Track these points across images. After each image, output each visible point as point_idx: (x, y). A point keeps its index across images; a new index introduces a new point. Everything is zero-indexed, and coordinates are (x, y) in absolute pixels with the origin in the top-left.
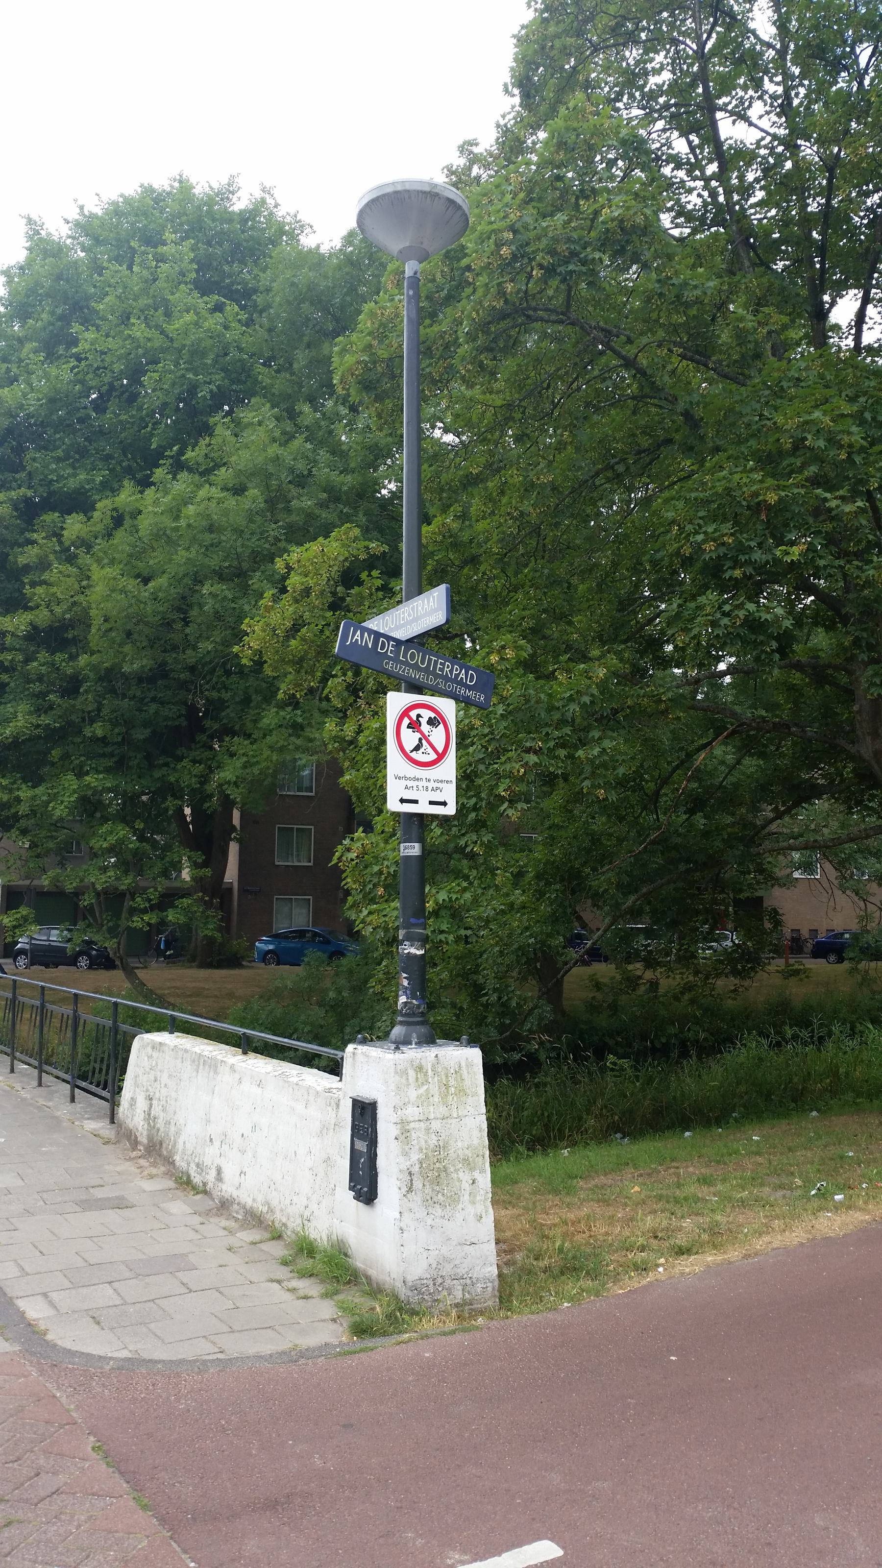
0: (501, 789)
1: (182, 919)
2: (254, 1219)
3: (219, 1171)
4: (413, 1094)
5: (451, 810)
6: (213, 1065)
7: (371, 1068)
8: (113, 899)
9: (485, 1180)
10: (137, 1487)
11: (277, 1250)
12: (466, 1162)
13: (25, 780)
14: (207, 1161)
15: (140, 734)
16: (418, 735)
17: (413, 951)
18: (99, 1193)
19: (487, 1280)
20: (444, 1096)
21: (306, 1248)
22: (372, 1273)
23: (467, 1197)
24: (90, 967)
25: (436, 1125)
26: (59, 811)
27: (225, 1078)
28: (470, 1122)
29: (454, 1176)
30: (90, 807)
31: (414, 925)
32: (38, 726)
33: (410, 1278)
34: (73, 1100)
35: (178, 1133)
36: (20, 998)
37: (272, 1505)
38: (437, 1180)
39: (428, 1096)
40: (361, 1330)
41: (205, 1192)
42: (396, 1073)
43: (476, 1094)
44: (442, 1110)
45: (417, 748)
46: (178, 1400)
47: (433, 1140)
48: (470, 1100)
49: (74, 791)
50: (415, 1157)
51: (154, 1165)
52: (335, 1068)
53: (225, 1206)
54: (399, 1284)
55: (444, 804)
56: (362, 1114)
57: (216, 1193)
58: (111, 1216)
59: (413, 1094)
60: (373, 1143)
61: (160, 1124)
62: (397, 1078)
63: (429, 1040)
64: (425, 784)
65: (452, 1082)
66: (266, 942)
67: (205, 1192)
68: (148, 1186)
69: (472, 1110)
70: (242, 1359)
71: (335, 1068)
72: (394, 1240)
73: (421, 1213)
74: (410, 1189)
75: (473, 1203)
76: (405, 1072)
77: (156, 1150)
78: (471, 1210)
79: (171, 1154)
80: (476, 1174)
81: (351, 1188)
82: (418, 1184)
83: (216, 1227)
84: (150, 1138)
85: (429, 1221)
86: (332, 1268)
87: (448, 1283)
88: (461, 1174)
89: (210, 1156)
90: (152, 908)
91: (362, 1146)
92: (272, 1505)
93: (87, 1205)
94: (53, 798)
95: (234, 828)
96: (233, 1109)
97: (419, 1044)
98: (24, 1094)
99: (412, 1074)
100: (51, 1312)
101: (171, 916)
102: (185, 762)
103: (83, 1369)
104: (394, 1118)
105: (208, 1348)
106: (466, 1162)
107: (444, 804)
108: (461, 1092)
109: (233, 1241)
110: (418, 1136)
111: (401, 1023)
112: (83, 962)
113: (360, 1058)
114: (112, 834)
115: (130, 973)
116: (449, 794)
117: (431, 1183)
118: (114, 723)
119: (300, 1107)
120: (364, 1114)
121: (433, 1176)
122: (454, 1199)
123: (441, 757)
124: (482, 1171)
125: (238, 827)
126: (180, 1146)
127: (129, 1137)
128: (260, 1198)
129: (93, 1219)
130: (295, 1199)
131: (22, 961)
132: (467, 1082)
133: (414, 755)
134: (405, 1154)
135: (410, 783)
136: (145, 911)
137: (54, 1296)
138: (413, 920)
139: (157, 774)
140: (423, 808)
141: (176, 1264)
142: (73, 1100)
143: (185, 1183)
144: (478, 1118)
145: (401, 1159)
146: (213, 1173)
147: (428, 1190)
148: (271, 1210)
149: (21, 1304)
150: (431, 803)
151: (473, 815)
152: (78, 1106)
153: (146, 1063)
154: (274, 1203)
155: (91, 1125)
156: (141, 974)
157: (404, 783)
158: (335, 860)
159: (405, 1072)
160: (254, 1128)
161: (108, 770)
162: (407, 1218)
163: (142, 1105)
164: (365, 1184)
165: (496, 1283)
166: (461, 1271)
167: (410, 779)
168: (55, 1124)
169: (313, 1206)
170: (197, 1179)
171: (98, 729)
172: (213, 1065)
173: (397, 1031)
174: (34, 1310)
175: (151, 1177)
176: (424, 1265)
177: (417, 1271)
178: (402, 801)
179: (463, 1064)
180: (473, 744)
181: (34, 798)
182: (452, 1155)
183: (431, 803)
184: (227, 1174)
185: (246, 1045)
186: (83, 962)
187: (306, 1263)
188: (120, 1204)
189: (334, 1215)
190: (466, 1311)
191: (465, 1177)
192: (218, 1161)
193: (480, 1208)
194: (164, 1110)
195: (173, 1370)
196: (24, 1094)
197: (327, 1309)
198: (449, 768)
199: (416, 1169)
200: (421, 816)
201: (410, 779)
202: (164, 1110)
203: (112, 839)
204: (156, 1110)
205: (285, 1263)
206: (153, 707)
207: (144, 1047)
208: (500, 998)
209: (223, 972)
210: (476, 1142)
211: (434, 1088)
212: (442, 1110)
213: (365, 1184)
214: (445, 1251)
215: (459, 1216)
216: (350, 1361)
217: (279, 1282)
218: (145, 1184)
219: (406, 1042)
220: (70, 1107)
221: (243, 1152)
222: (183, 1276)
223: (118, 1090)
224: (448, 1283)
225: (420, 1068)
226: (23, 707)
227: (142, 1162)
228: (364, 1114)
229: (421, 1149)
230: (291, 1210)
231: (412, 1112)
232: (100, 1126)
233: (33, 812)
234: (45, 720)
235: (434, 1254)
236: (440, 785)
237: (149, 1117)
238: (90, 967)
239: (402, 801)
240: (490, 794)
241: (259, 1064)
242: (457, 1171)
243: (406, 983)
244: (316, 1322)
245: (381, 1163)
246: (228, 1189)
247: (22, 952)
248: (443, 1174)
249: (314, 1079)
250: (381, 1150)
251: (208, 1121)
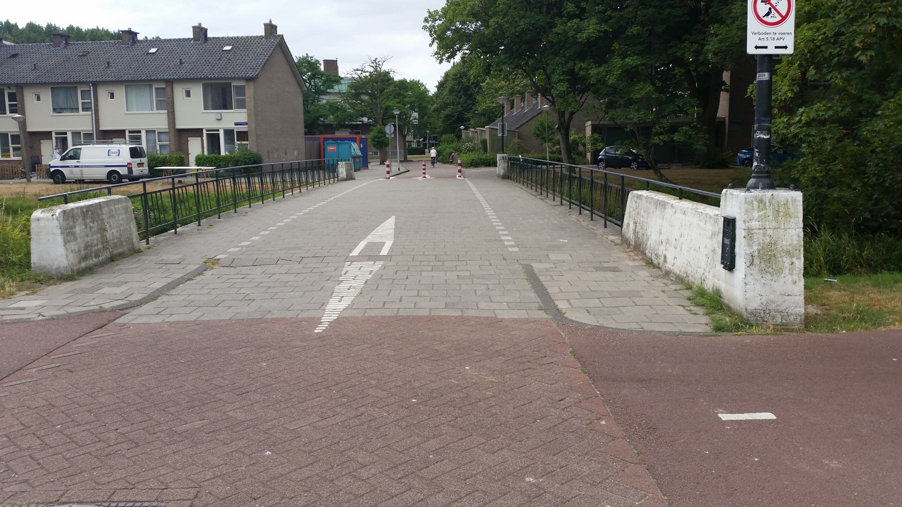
0: (857, 42)
1: (682, 139)
2: (680, 280)
3: (665, 257)
4: (756, 215)
5: (790, 51)
6: (663, 205)
7: (734, 201)
8: (646, 129)
9: (800, 263)
10: (584, 364)
11: (688, 293)
12: (789, 253)
13: (595, 63)
14: (660, 253)
15: (659, 29)
16: (769, 6)
17: (762, 136)
18: (606, 265)
19: (796, 314)
20: (776, 217)
21: (702, 293)
22: (732, 305)
23: (787, 271)
24: (638, 168)
25: (769, 232)
26: (611, 80)
27: (669, 211)
28: (793, 233)
29: (780, 259)
30: (631, 76)
31: (764, 121)
32: (600, 31)
33: (749, 308)
34: (606, 226)
35: (647, 239)
36: (595, 180)
37: (641, 381)
38: (769, 261)
39: (766, 216)
40: (719, 329)
41: (659, 268)
42: (746, 203)
43: (797, 217)
44: (774, 224)
45: (768, 14)
46: (613, 341)
47: (768, 240)
48: (793, 220)
49: (620, 68)
50: (755, 248)
51: (636, 255)
52: (716, 203)
53: (667, 274)
54: (744, 311)
55: (786, 47)
56: (728, 225)
57: (663, 268)
58: (609, 274)
59: (756, 215)
60: (733, 239)
61: (640, 235)
62: (747, 206)
63: (772, 187)
64: (772, 36)
65: (782, 209)
66: (745, 153)
67: (659, 268)
68: (631, 263)
69: (794, 226)
70: (651, 331)
71: (716, 203)
72: (741, 288)
73: (758, 276)
74: (752, 264)
75: (791, 274)
76: (751, 203)
77: (637, 248)
78: (789, 278)
79: (645, 249)
80: (794, 260)
81: (722, 263)
82: (757, 261)
83: (659, 283)
84: (635, 242)
85: (763, 281)
86: (712, 302)
87: (773, 313)
88: (784, 259)
89: (661, 250)
90: (666, 132)
91: (727, 242)
92: (641, 381)
93: (598, 269)
94: (608, 73)
95: (724, 83)
96: (674, 227)
97: (763, 188)
98: (583, 223)
99: (756, 204)
100: (569, 306)
101: (676, 137)
102: (686, 44)
103: (577, 327)
104: (743, 226)
105: (637, 326)
106: (789, 253)
107: (786, 47)
108: (787, 215)
109: (666, 289)
110: (758, 236)
111: (754, 177)
112: (634, 165)
113: (729, 196)
114: (644, 89)
115: (657, 171)
116: (789, 42)
117: (765, 261)
118: (642, 24)
119: (702, 224)
120: (729, 224)
121: (767, 258)
122: (780, 271)
123: (784, 18)
124: (798, 258)
125: (728, 83)
126: (648, 246)
127: (625, 241)
128: (683, 270)
129: (600, 275)
130: (699, 270)
131: (602, 165)
132: (792, 210)
133: (765, 19)
134: (750, 246)
135: (762, 36)
136: (661, 134)
137: (572, 301)
138: (762, 118)
139: (670, 52)
140: (771, 51)
141: (633, 294)
142: (606, 226)
143: (650, 263)
144: (798, 230)
145: (747, 248)
146: (662, 258)
147: (763, 265)
148: (687, 276)
149: (557, 303)
150: (776, 47)
151: (836, 59)
152: (608, 230)
153: (634, 205)
154: (689, 272)
155: (611, 238)
156: (662, 171)
157: (758, 36)
158: (749, 94)
159: (751, 203)
160: (681, 236)
161: (641, 54)
162: (749, 278)
163: (632, 226)
164: (729, 263)
165: (803, 317)
166: (781, 308)
167: (762, 34)
168: (595, 236)
169: (706, 273)
170: (655, 262)
171: (635, 29)
172: (663, 205)
173: (752, 181)
174: (562, 305)
175: (634, 260)
176: (759, 302)
177: (754, 305)
178: (757, 47)
179: (790, 200)
180: (840, 13)
181: (598, 74)
182: (779, 248)
183: (776, 47)
184: (669, 259)
185: (682, 195)
186: (634, 165)
187: (699, 299)
188: (615, 270)
189: (714, 277)
190: (784, 328)
191: (787, 261)
192: (665, 253)
193: (795, 278)
194: (642, 228)
195: (615, 332)
196: (583, 223)
197: (705, 319)
198: (790, 24)
199: (756, 254)
200: (770, 56)
201: (762, 34)
202: (642, 228)
203: (643, 93)
204: (639, 229)
205: (689, 299)
206: (668, 10)
207: (633, 197)
208: (878, 180)
209: (715, 171)
210: (795, 242)
211: (770, 212)
212: (774, 224)
213: (729, 263)
214: (772, 297)
215: (782, 280)
216: (706, 339)
217: (684, 307)
218: (628, 262)
219: (755, 187)
220: (604, 229)
221: (676, 248)
222: (635, 299)
223: (622, 218)
224: (773, 313)
225: (761, 201)
226: (594, 20)
227: (631, 254)
228: (729, 224)
229: (759, 244)
230: (697, 276)
231: (755, 224)
232: (616, 239)
233: (599, 81)
234: (604, 27)
235: (764, 298)
236: (783, 36)
237: (635, 232)
238: (638, 168)
239: (757, 47)
240: (850, 45)
241: (686, 204)
242: (782, 257)
243: (757, 154)
244: (699, 323)
245: (737, 250)
246: (669, 266)
247: (601, 160)
248: (773, 258)
249: (710, 210)
250: (737, 244)
251: (661, 233)
